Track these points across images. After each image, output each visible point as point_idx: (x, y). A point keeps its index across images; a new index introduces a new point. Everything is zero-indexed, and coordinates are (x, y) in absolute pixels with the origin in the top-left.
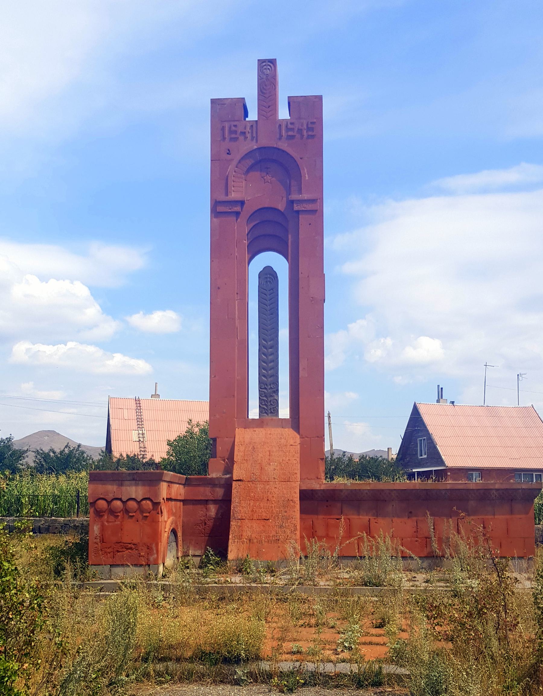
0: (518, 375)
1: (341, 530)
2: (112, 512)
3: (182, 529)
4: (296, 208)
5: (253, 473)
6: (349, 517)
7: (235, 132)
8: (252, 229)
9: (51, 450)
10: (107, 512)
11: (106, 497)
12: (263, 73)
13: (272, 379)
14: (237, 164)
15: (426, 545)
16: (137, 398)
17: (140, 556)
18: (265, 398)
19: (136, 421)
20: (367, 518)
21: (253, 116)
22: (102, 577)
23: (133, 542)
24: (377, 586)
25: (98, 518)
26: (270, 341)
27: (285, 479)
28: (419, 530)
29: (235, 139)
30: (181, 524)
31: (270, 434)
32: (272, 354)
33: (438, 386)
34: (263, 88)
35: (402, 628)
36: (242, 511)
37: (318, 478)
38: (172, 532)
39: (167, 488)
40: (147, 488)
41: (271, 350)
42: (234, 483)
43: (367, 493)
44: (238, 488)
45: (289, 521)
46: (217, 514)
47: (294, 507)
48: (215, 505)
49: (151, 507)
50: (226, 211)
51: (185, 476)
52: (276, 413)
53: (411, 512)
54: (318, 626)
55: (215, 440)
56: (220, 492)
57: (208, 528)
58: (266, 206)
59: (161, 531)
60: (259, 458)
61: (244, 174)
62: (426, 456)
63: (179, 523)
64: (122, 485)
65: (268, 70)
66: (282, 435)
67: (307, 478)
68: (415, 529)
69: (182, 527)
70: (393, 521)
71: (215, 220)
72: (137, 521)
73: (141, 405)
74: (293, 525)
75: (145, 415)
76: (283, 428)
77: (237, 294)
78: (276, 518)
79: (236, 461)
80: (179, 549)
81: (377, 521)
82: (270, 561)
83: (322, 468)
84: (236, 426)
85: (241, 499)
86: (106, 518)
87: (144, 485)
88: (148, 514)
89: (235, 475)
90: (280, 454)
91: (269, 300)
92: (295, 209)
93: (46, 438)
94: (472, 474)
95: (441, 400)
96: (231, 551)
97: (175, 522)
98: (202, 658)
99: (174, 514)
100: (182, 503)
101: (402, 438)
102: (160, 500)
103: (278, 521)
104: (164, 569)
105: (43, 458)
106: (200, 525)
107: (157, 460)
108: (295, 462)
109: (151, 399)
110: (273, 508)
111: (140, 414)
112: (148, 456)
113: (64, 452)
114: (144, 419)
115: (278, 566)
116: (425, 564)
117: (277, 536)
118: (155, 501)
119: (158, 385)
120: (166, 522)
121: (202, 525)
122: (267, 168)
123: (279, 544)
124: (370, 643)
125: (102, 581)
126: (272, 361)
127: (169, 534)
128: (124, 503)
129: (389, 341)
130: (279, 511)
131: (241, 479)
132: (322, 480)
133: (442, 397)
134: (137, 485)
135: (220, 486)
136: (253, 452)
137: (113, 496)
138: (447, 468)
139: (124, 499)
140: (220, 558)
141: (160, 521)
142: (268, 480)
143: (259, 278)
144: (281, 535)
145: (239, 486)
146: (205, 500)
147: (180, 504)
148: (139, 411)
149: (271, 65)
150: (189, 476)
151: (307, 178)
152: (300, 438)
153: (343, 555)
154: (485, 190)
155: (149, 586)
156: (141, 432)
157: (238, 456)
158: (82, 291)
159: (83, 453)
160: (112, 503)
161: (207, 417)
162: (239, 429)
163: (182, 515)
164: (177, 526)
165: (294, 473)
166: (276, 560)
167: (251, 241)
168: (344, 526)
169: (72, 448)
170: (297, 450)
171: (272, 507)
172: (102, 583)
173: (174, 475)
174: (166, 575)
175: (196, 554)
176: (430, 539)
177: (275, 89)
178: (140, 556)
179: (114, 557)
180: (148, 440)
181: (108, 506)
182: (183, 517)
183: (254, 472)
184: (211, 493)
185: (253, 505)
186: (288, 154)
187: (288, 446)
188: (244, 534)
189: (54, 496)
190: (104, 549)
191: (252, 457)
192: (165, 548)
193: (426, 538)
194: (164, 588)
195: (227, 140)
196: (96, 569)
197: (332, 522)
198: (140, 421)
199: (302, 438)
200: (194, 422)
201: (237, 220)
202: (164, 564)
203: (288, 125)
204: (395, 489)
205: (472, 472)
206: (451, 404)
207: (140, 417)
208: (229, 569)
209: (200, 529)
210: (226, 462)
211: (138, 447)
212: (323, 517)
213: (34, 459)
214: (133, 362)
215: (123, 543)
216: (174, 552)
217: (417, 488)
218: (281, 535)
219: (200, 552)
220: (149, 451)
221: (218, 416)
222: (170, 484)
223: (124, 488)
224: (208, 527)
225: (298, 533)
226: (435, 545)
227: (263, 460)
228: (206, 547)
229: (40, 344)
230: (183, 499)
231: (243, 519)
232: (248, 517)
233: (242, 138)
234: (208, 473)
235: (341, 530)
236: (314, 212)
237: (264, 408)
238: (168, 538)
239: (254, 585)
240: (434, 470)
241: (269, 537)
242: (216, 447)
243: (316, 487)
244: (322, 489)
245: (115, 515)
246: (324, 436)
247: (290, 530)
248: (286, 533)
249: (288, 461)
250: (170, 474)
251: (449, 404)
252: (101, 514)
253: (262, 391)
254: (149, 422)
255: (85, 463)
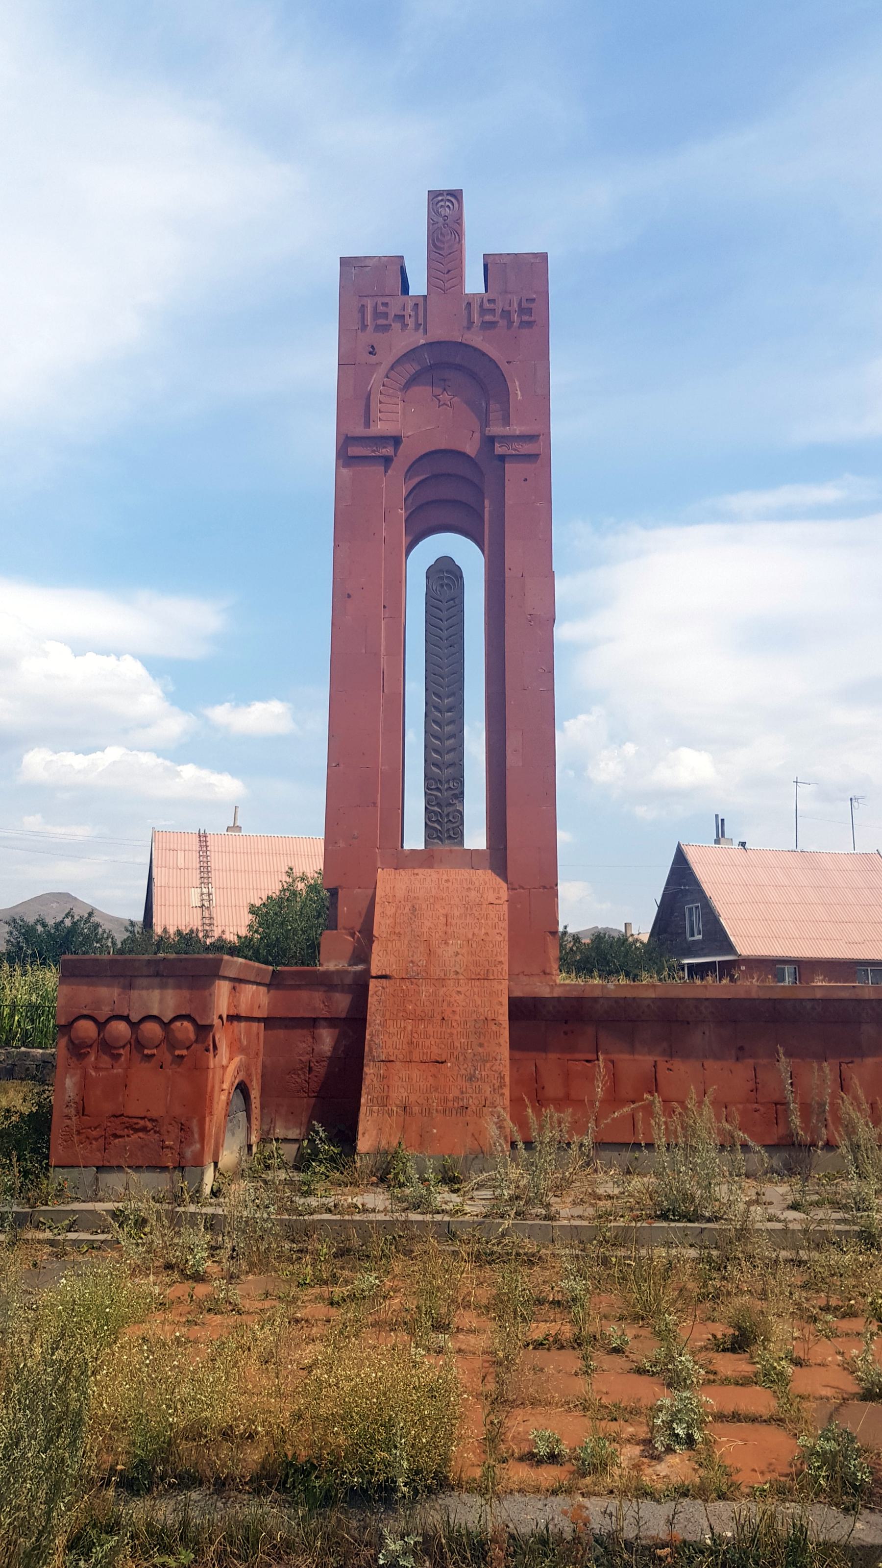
0: (851, 799)
1: (598, 1087)
2: (107, 1047)
3: (260, 1081)
4: (499, 450)
5: (412, 962)
6: (614, 1057)
7: (386, 315)
8: (414, 488)
9: (38, 921)
10: (95, 1047)
11: (95, 1014)
12: (438, 213)
13: (450, 770)
14: (389, 371)
15: (776, 1118)
16: (202, 832)
17: (163, 1148)
18: (436, 809)
19: (198, 871)
20: (650, 1059)
21: (418, 285)
22: (76, 1194)
23: (148, 1114)
24: (690, 1221)
25: (74, 1059)
26: (448, 698)
27: (479, 974)
28: (759, 1086)
29: (386, 328)
30: (259, 1071)
31: (447, 881)
32: (452, 722)
33: (717, 816)
34: (438, 239)
35: (794, 1356)
36: (389, 1043)
37: (545, 973)
38: (238, 1091)
39: (231, 993)
40: (186, 993)
41: (449, 714)
42: (373, 983)
43: (649, 1006)
44: (380, 993)
45: (488, 1065)
46: (335, 1048)
47: (497, 1035)
48: (331, 1030)
49: (192, 1036)
50: (367, 454)
51: (271, 968)
52: (459, 839)
53: (741, 1048)
54: (580, 1345)
55: (334, 893)
56: (342, 1002)
57: (315, 1079)
58: (443, 447)
59: (213, 1087)
60: (425, 930)
61: (401, 390)
62: (700, 937)
63: (253, 1070)
64: (131, 987)
65: (447, 209)
66: (471, 882)
67: (523, 972)
68: (751, 1085)
69: (262, 1076)
70: (705, 1066)
71: (345, 471)
72: (161, 1067)
73: (208, 844)
74: (496, 1076)
75: (216, 861)
76: (473, 868)
77: (384, 607)
78: (461, 1058)
79: (377, 936)
80: (254, 1127)
81: (671, 1067)
82: (449, 1156)
83: (554, 953)
84: (379, 865)
85: (387, 1017)
86: (93, 1059)
87: (179, 987)
88: (184, 1052)
89: (375, 966)
90: (467, 922)
91: (447, 610)
92: (496, 452)
93: (54, 905)
94: (784, 969)
95: (722, 840)
96: (364, 1134)
97: (246, 1068)
98: (285, 1482)
99: (243, 1050)
100: (263, 1024)
101: (659, 904)
102: (213, 1020)
103: (466, 1066)
104: (217, 1175)
105: (24, 936)
106: (299, 1072)
107: (230, 937)
108: (499, 938)
109: (226, 833)
110: (455, 1037)
111: (205, 859)
112: (217, 933)
113: (63, 925)
114: (213, 867)
115: (466, 1168)
116: (777, 1163)
117: (462, 1100)
118: (203, 1023)
119: (239, 810)
120: (224, 1068)
121: (304, 1073)
122: (445, 380)
123: (468, 1118)
124: (736, 1417)
125: (76, 1206)
126: (453, 736)
127: (231, 1095)
128: (134, 1026)
129: (630, 749)
130: (466, 1044)
131: (388, 973)
132: (553, 978)
133: (723, 836)
134: (163, 987)
135: (344, 988)
136: (413, 917)
137: (112, 1011)
138: (740, 958)
139: (135, 1018)
140: (340, 1149)
141: (212, 1066)
142: (443, 977)
143: (427, 578)
144: (472, 1097)
145: (383, 988)
146: (311, 1018)
147: (258, 1028)
148: (205, 854)
149: (453, 200)
150: (278, 968)
151: (519, 398)
152: (508, 889)
153: (602, 1139)
154: (785, 515)
155: (175, 1220)
156: (205, 891)
157: (381, 926)
158: (132, 669)
159: (97, 926)
160: (108, 1027)
161: (319, 865)
162: (385, 870)
163: (262, 1049)
164: (249, 1075)
165: (497, 963)
166: (461, 1153)
167: (413, 511)
168: (604, 1077)
169: (76, 918)
170: (502, 913)
171: (451, 1034)
172: (74, 1212)
173: (246, 965)
174: (219, 1190)
175: (289, 1137)
176: (784, 1107)
177: (460, 241)
178: (163, 1148)
179: (105, 1149)
180: (218, 905)
181: (99, 1035)
182: (264, 1055)
183: (415, 958)
184: (324, 1003)
185: (412, 1031)
186: (484, 354)
187: (485, 906)
188: (393, 1095)
189: (30, 1005)
190: (84, 1131)
191: (410, 929)
192: (219, 1127)
193: (776, 1104)
194: (212, 1224)
195: (370, 328)
196: (65, 1176)
197: (578, 1067)
198: (205, 872)
199: (513, 889)
200: (297, 872)
201: (386, 472)
202: (216, 1164)
203: (485, 305)
204: (707, 997)
205: (783, 966)
206: (740, 847)
207: (205, 865)
208: (359, 1174)
209: (299, 1080)
210: (356, 937)
211: (200, 917)
212: (559, 1056)
213: (8, 938)
214: (215, 778)
215: (129, 1117)
216: (241, 1135)
217: (754, 995)
218: (472, 1097)
219: (298, 1131)
220: (219, 924)
221: (342, 844)
222: (237, 984)
223: (135, 994)
224: (316, 1076)
225: (506, 1091)
226: (796, 1120)
227: (433, 934)
228: (310, 1122)
229: (64, 753)
230: (266, 1016)
231: (390, 1061)
232: (401, 1057)
233: (396, 326)
234: (319, 961)
235: (598, 1087)
236: (533, 457)
237: (435, 829)
238: (228, 1104)
239: (414, 1217)
240: (719, 962)
241: (446, 1100)
242: (337, 908)
243: (545, 992)
244: (555, 995)
245: (113, 1053)
246: (557, 885)
247: (491, 1084)
248: (483, 1091)
249: (484, 937)
250: (236, 962)
251: (737, 847)
252: (82, 1051)
253: (431, 794)
254: (221, 873)
255: (98, 945)
